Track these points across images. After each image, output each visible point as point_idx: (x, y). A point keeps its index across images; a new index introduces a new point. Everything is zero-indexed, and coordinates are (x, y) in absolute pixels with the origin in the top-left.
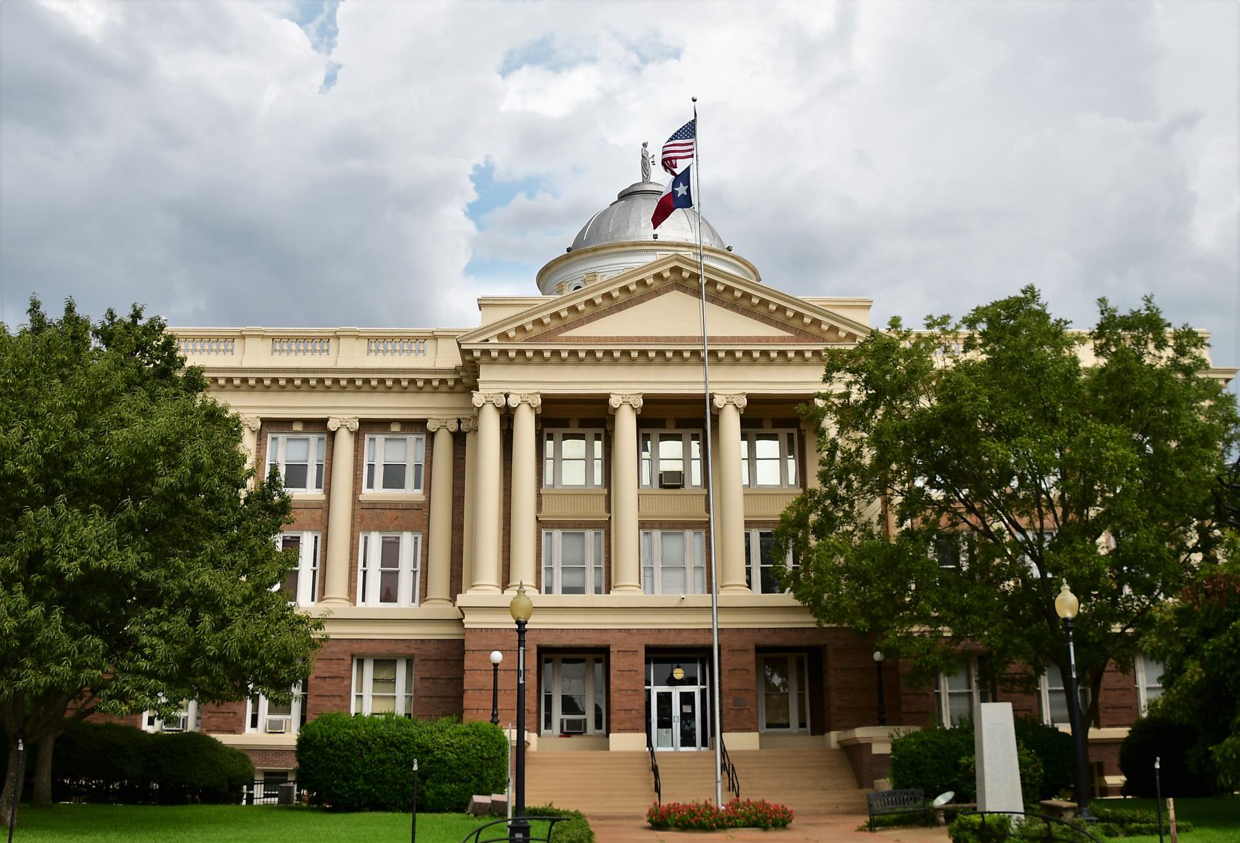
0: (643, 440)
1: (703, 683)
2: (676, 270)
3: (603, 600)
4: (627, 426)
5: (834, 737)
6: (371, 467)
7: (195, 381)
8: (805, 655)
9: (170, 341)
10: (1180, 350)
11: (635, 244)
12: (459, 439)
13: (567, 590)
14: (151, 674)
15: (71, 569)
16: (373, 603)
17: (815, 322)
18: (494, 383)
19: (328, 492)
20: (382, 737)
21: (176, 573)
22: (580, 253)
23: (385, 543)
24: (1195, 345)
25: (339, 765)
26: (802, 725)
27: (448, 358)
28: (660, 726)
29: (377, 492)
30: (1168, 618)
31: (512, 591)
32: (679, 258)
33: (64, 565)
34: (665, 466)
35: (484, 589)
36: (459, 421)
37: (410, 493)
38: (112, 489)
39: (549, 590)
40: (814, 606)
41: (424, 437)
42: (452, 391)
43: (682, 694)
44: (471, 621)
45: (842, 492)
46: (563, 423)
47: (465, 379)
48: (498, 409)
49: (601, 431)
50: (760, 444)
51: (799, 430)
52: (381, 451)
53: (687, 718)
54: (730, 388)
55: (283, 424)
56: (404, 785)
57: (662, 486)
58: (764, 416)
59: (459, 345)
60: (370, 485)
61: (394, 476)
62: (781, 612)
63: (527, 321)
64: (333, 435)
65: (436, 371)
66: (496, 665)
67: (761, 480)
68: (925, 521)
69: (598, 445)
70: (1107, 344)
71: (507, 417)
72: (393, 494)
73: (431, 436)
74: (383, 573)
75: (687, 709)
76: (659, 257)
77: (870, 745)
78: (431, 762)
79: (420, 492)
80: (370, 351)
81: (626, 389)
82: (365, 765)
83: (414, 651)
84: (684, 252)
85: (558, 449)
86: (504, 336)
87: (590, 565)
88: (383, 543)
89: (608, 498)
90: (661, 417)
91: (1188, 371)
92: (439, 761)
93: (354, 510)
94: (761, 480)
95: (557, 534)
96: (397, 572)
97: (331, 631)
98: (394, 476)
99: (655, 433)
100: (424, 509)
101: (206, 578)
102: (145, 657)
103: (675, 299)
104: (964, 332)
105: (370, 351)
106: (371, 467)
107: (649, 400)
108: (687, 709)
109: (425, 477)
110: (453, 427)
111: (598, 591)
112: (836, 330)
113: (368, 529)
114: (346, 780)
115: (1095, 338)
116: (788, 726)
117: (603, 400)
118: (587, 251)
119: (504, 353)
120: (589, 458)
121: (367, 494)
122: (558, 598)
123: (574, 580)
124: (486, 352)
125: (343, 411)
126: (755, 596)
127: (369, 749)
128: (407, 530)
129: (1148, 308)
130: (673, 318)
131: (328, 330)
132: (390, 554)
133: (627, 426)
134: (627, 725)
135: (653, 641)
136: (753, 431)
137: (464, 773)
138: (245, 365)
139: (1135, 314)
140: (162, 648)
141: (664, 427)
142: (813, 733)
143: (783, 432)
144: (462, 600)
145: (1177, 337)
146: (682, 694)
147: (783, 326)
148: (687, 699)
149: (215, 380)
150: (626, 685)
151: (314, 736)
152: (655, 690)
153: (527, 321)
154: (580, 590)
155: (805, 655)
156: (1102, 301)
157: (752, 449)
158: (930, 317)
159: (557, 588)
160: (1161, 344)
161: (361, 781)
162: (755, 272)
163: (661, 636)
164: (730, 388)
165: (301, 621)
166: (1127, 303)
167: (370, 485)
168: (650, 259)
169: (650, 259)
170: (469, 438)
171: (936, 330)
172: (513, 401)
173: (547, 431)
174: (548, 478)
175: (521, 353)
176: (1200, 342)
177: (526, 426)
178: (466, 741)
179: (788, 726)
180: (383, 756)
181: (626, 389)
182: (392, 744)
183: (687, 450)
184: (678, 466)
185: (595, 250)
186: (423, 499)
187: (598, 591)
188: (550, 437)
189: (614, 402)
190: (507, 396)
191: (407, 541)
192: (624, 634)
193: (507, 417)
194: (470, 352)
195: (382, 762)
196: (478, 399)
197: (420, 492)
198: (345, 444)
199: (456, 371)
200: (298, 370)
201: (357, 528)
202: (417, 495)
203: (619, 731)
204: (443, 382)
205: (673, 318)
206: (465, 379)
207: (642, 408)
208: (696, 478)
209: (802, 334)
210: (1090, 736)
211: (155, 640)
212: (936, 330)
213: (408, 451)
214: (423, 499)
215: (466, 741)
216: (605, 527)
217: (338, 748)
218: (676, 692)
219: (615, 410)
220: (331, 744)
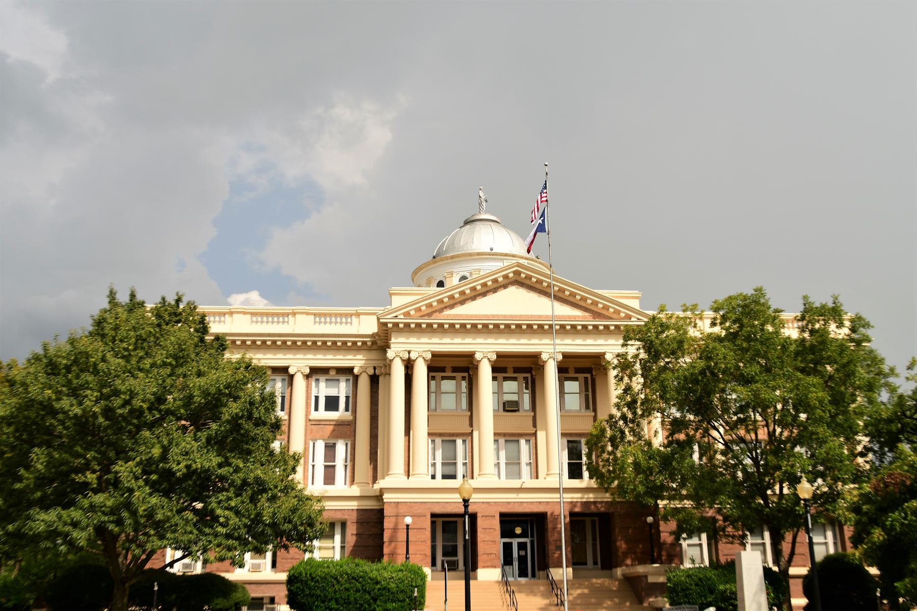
0: (430, 378)
1: (532, 536)
2: (517, 273)
5: (619, 572)
6: (317, 398)
7: (221, 343)
8: (597, 519)
9: (203, 317)
10: (853, 330)
11: (479, 254)
12: (374, 380)
13: (445, 477)
14: (228, 536)
15: (179, 469)
17: (606, 308)
18: (398, 347)
20: (347, 574)
21: (237, 470)
22: (442, 260)
23: (327, 446)
24: (864, 327)
25: (318, 592)
26: (595, 563)
27: (368, 326)
30: (855, 499)
31: (414, 479)
32: (519, 265)
33: (175, 467)
34: (507, 398)
35: (394, 478)
36: (375, 368)
38: (201, 413)
39: (433, 477)
40: (604, 486)
42: (370, 349)
43: (519, 544)
44: (387, 497)
45: (630, 416)
46: (442, 369)
47: (379, 344)
48: (403, 361)
49: (466, 374)
50: (567, 383)
51: (592, 375)
52: (324, 390)
53: (522, 560)
54: (551, 350)
55: (324, 371)
56: (362, 605)
57: (505, 410)
59: (378, 319)
60: (316, 409)
61: (332, 403)
62: (582, 490)
64: (292, 377)
66: (408, 526)
68: (687, 435)
69: (464, 384)
70: (807, 325)
71: (409, 366)
72: (333, 415)
73: (356, 378)
74: (325, 466)
75: (522, 553)
76: (506, 264)
77: (646, 577)
78: (379, 589)
79: (349, 413)
80: (253, 322)
81: (485, 349)
82: (335, 592)
83: (346, 517)
84: (522, 261)
85: (438, 386)
86: (407, 314)
87: (460, 460)
88: (326, 447)
89: (471, 417)
91: (858, 343)
92: (384, 588)
93: (306, 425)
96: (334, 466)
97: (329, 505)
98: (332, 403)
99: (439, 375)
101: (259, 472)
102: (222, 525)
103: (514, 292)
104: (711, 314)
105: (315, 322)
106: (317, 398)
107: (500, 356)
108: (522, 553)
110: (371, 372)
112: (619, 312)
114: (323, 602)
115: (799, 320)
116: (586, 564)
117: (470, 356)
118: (447, 258)
119: (407, 325)
120: (458, 392)
121: (314, 415)
122: (440, 482)
123: (449, 470)
124: (396, 325)
125: (299, 363)
127: (338, 582)
128: (341, 438)
129: (834, 303)
130: (516, 303)
131: (351, 310)
133: (485, 372)
134: (489, 564)
135: (505, 510)
136: (500, 376)
137: (401, 596)
138: (297, 332)
139: (823, 307)
140: (234, 520)
141: (444, 371)
142: (603, 568)
143: (581, 376)
144: (381, 484)
145: (852, 321)
146: (519, 544)
147: (586, 309)
148: (522, 546)
149: (234, 342)
150: (488, 538)
151: (300, 574)
154: (453, 477)
155: (597, 519)
156: (805, 298)
157: (500, 387)
158: (684, 305)
159: (439, 475)
160: (840, 325)
161: (333, 602)
163: (509, 506)
164: (551, 350)
165: (308, 499)
166: (820, 299)
167: (316, 409)
168: (498, 265)
169: (498, 265)
170: (381, 379)
171: (689, 314)
172: (413, 356)
175: (418, 325)
176: (867, 325)
178: (400, 575)
179: (586, 564)
180: (347, 586)
181: (485, 349)
182: (353, 578)
183: (458, 386)
184: (514, 398)
185: (452, 257)
186: (351, 418)
188: (433, 378)
189: (478, 356)
190: (409, 352)
191: (341, 449)
192: (485, 505)
193: (409, 366)
194: (386, 324)
195: (347, 590)
196: (390, 354)
197: (349, 413)
198: (300, 383)
200: (269, 335)
201: (308, 437)
202: (348, 416)
203: (484, 567)
204: (364, 343)
205: (516, 303)
206: (379, 344)
207: (431, 360)
209: (597, 315)
211: (227, 512)
212: (689, 314)
213: (342, 390)
214: (351, 418)
215: (400, 575)
217: (318, 581)
218: (515, 542)
219: (391, 361)
220: (312, 579)
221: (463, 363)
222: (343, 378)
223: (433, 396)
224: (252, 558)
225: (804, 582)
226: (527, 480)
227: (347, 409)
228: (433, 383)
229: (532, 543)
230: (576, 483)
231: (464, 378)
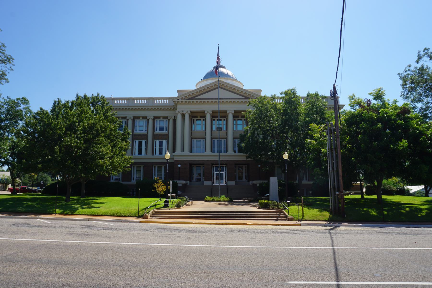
0: (234, 120)
3: (226, 154)
4: (208, 117)
5: (251, 183)
16: (149, 155)
19: (148, 132)
28: (216, 180)
29: (158, 132)
35: (178, 152)
37: (165, 132)
39: (221, 152)
41: (156, 120)
46: (238, 117)
47: (175, 108)
49: (225, 118)
58: (237, 115)
62: (241, 157)
63: (187, 95)
65: (169, 106)
67: (238, 129)
71: (183, 115)
72: (161, 132)
85: (236, 122)
89: (227, 133)
90: (214, 115)
94: (238, 129)
95: (195, 140)
99: (236, 119)
100: (168, 135)
109: (167, 129)
111: (218, 152)
113: (156, 139)
121: (156, 132)
126: (233, 154)
132: (140, 144)
133: (208, 117)
152: (215, 172)
153: (187, 95)
159: (237, 151)
162: (242, 84)
167: (157, 130)
172: (184, 113)
173: (213, 118)
174: (193, 128)
177: (187, 117)
187: (224, 152)
188: (235, 120)
189: (228, 112)
191: (164, 142)
193: (183, 115)
198: (130, 122)
199: (173, 106)
208: (225, 129)
210: (205, 184)
213: (164, 124)
216: (227, 138)
221: (202, 115)
222: (165, 120)
223: (235, 126)
224: (140, 179)
225: (141, 198)
226: (151, 156)
227: (166, 130)
228: (235, 121)
229: (225, 173)
230: (213, 154)
231: (224, 120)
